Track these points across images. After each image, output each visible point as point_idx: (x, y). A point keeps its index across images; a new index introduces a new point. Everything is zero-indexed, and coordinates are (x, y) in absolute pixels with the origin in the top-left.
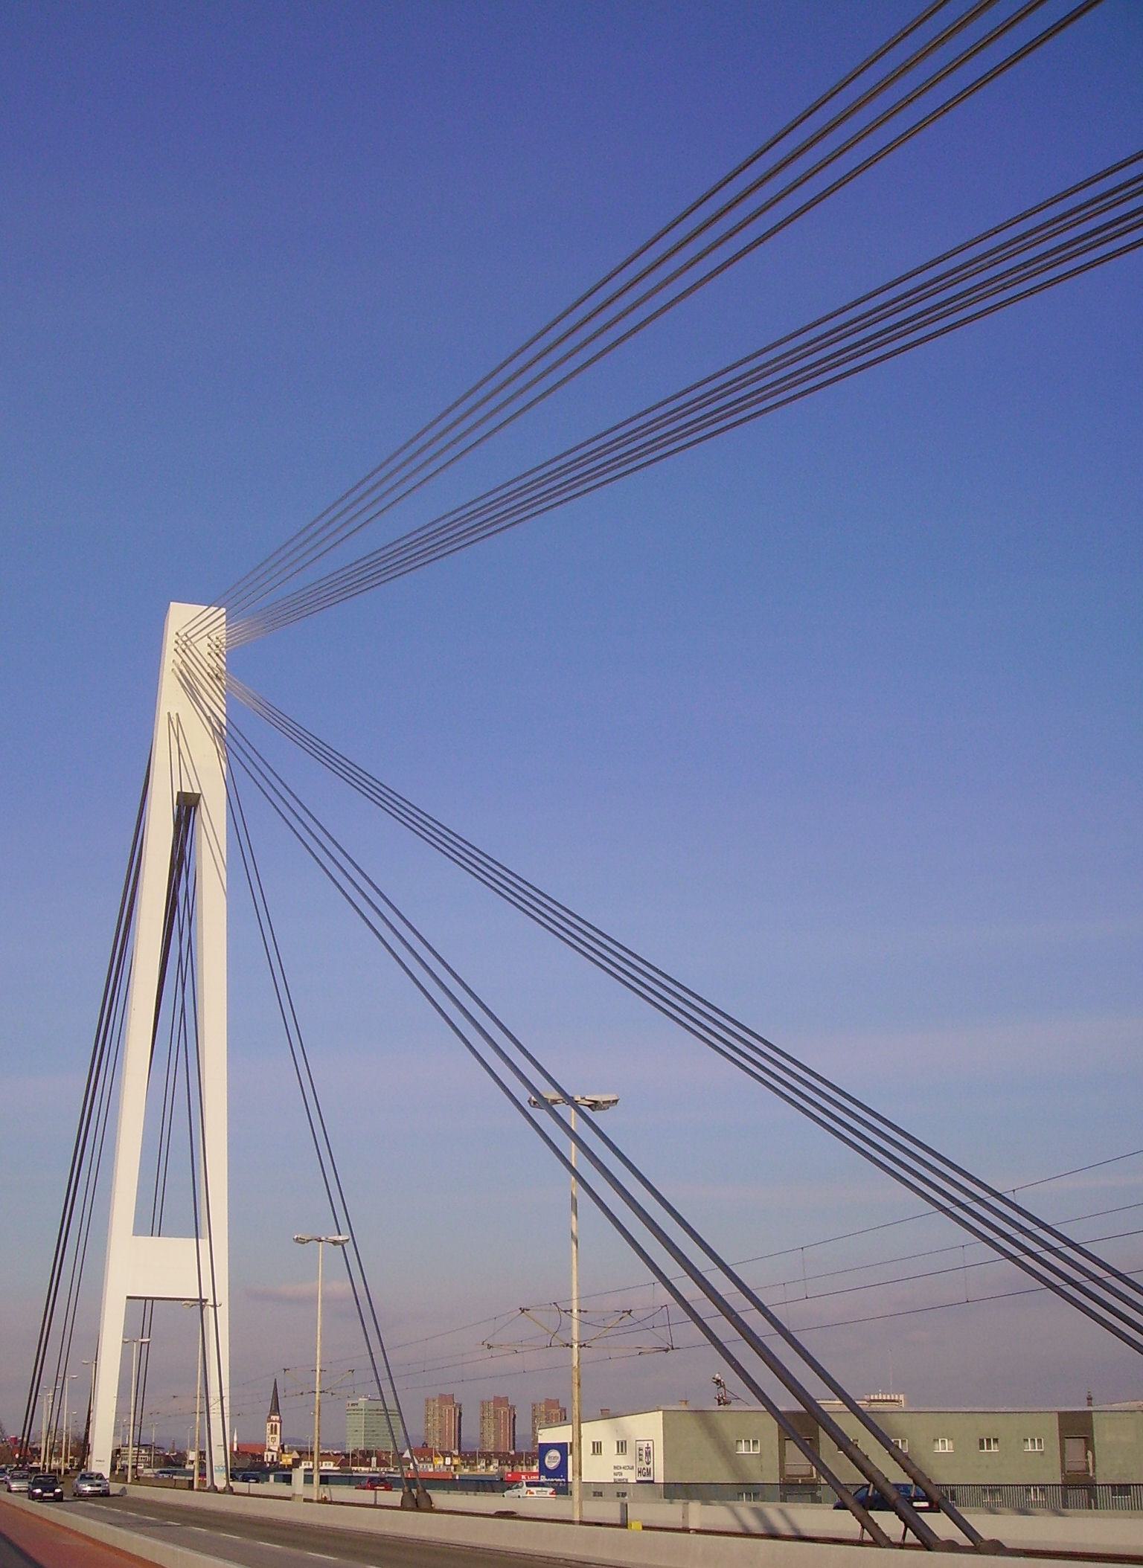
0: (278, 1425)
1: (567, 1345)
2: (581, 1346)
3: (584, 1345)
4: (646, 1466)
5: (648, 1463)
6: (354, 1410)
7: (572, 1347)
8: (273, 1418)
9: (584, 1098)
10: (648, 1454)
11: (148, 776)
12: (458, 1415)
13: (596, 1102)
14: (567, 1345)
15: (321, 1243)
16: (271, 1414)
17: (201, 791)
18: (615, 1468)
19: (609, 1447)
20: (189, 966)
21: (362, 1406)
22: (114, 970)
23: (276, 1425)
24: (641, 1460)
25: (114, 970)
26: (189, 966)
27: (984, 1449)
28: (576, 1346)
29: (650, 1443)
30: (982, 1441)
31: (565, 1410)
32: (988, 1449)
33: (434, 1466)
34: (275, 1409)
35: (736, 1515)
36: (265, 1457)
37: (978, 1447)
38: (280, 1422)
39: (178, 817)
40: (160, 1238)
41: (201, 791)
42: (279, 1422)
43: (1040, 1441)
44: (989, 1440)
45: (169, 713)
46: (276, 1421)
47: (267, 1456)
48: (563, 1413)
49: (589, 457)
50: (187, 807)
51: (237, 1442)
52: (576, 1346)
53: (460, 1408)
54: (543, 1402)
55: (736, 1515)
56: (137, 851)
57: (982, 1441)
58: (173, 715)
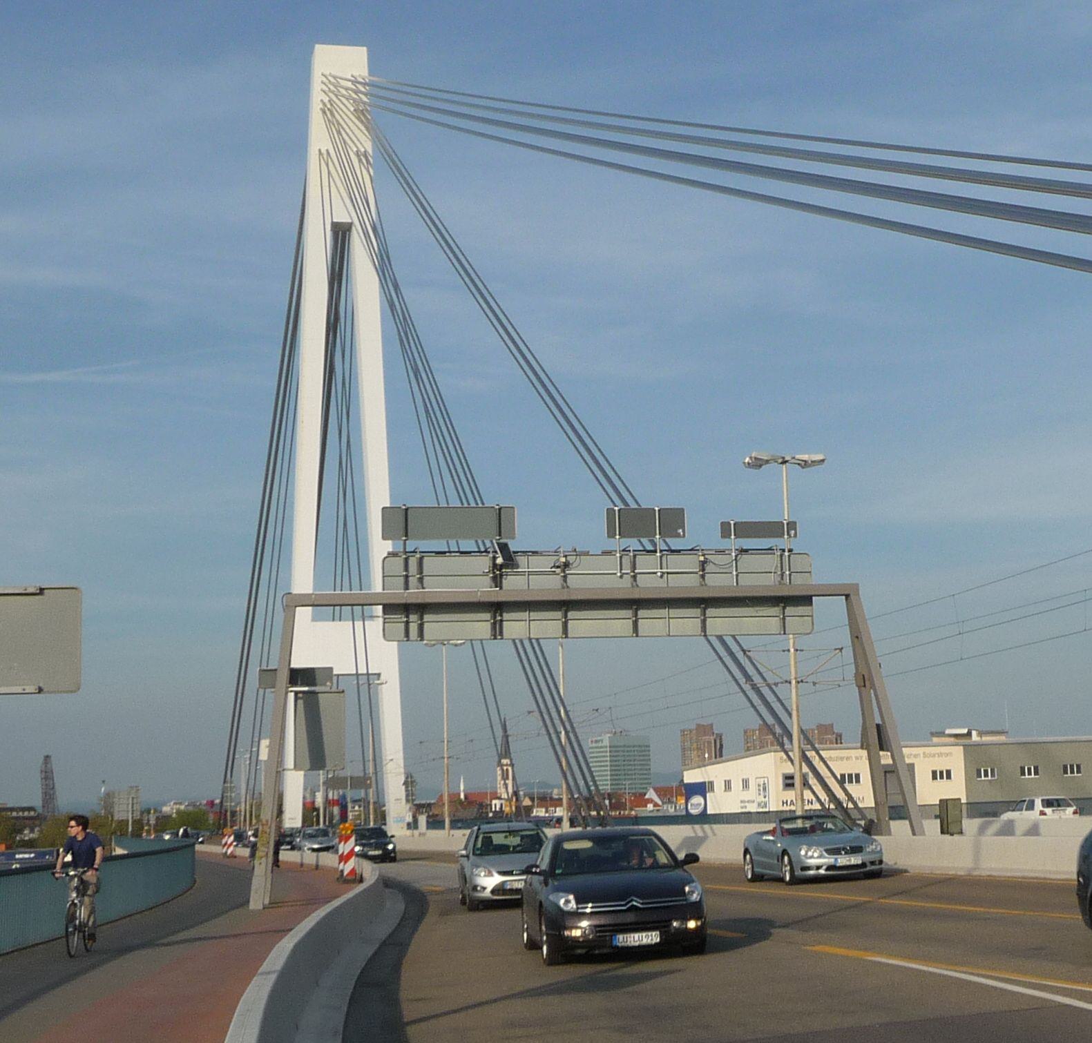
0: (510, 768)
1: (786, 682)
2: (798, 682)
3: (802, 681)
4: (763, 800)
5: (765, 797)
6: (596, 748)
7: (790, 683)
8: (505, 761)
9: (794, 458)
10: (765, 789)
11: (304, 195)
12: (718, 747)
13: (805, 461)
14: (786, 682)
15: (444, 648)
16: (501, 757)
17: (351, 219)
18: (742, 802)
19: (737, 785)
20: (349, 471)
21: (606, 743)
22: (284, 375)
23: (507, 770)
24: (760, 794)
25: (284, 375)
26: (349, 471)
27: (981, 777)
28: (794, 682)
29: (766, 780)
30: (1065, 767)
31: (840, 736)
32: (1077, 773)
33: (675, 807)
34: (506, 752)
35: (695, 832)
36: (493, 806)
37: (975, 776)
38: (512, 765)
39: (332, 274)
40: (342, 622)
41: (351, 219)
42: (510, 765)
43: (992, 771)
44: (1072, 767)
45: (320, 151)
46: (507, 765)
47: (495, 805)
48: (839, 739)
49: (463, 461)
50: (341, 233)
51: (464, 791)
52: (794, 682)
53: (721, 739)
54: (814, 727)
55: (695, 832)
56: (297, 283)
57: (1065, 767)
58: (324, 151)
